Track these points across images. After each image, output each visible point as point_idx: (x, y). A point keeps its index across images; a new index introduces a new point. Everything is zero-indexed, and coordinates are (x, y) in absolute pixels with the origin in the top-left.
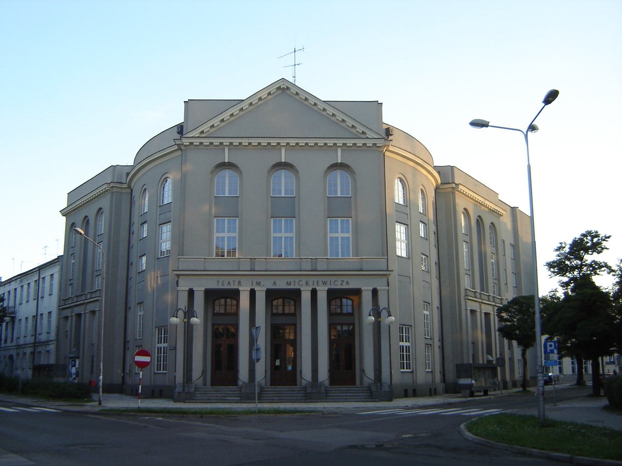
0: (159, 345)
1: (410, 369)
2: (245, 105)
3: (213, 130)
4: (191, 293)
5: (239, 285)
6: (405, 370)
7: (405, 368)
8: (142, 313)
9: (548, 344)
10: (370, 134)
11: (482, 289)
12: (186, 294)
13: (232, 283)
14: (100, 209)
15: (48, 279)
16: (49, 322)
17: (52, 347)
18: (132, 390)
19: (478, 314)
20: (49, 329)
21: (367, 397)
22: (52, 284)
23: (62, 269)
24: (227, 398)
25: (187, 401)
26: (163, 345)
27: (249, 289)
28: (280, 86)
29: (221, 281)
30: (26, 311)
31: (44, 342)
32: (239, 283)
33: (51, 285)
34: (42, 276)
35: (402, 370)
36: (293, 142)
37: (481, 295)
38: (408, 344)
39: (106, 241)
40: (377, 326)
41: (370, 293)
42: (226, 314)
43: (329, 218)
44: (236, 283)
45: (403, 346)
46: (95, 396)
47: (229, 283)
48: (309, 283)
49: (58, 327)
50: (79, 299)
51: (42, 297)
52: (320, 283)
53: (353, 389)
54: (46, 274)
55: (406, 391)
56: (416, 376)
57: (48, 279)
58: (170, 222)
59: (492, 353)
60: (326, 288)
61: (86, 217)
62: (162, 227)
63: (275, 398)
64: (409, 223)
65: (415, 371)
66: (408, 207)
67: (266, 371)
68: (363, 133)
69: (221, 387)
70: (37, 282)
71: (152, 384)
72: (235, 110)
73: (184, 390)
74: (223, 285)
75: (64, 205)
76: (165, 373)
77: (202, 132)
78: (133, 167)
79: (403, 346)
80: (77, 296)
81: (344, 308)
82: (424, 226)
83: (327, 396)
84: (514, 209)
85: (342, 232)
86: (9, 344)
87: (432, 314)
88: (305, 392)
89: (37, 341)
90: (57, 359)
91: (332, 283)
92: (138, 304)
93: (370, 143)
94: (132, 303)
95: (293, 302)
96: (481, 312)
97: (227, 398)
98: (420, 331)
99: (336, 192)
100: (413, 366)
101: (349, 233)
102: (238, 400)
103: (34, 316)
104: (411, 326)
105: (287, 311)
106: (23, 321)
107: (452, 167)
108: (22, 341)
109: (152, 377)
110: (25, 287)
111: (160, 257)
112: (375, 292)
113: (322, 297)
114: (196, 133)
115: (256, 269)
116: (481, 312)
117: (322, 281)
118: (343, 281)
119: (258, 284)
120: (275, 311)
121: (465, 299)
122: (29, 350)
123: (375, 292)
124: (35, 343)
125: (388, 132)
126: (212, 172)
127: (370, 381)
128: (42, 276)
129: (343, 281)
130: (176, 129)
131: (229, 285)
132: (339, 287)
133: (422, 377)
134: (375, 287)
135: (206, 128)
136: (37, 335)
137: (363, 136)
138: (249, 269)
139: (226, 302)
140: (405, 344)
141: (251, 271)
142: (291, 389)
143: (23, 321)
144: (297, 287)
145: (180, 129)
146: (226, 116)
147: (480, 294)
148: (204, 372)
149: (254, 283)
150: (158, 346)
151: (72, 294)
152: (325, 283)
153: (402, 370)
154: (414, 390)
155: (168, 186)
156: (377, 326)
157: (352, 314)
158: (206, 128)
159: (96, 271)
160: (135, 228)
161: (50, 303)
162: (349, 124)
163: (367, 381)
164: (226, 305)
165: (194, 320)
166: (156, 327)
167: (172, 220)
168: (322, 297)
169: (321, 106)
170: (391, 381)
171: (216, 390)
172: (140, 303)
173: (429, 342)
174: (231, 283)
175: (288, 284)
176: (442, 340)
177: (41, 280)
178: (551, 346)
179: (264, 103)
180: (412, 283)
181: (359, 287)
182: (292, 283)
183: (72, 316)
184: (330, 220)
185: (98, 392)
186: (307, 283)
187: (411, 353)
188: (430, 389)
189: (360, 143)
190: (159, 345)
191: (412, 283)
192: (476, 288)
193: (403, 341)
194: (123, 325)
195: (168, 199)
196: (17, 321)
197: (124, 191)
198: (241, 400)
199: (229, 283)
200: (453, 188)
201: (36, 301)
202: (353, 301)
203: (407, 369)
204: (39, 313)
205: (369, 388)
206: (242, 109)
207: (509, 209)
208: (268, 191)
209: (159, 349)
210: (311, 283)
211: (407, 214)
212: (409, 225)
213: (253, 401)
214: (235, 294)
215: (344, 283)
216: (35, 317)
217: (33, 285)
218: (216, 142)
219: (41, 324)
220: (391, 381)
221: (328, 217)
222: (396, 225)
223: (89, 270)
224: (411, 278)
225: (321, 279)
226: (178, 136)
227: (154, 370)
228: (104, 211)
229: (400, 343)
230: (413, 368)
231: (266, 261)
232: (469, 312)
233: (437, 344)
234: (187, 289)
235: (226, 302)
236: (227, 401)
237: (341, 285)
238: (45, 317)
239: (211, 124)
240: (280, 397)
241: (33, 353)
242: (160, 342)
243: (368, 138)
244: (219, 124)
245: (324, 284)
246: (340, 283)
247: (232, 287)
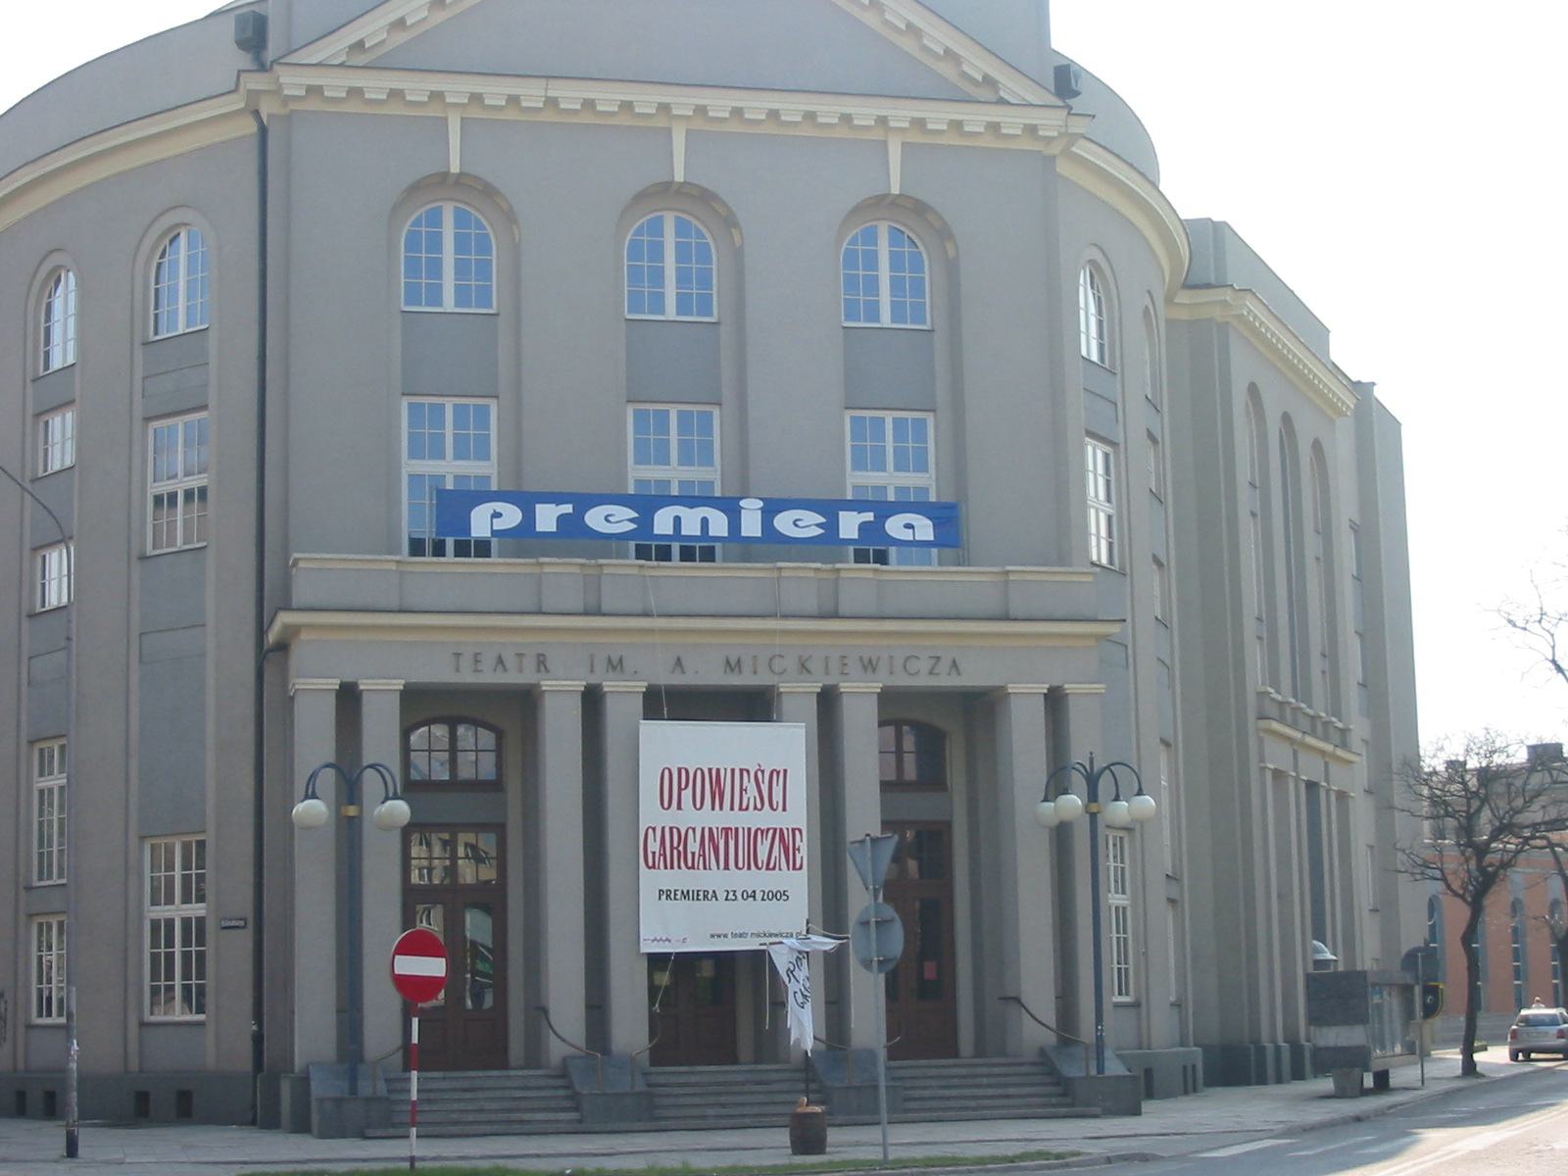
1: (1127, 994)
3: (401, 37)
4: (349, 698)
5: (539, 671)
8: (56, 781)
10: (1012, 86)
12: (330, 704)
13: (510, 661)
21: (1054, 1100)
24: (527, 1116)
25: (370, 1132)
26: (178, 911)
32: (541, 662)
38: (196, 910)
41: (1040, 704)
43: (405, 398)
44: (530, 663)
45: (170, 924)
48: (809, 665)
53: (985, 1070)
55: (21, 1096)
56: (1149, 1028)
59: (1324, 935)
62: (47, 423)
63: (710, 1112)
64: (1121, 439)
65: (1144, 1001)
66: (1119, 377)
68: (989, 82)
69: (481, 1074)
71: (21, 1066)
74: (476, 671)
76: (201, 1024)
77: (359, 46)
79: (170, 924)
81: (466, 760)
82: (1106, 456)
85: (460, 455)
88: (569, 1092)
95: (493, 735)
97: (527, 1116)
100: (1137, 983)
101: (487, 458)
102: (570, 1122)
105: (466, 772)
109: (133, 1047)
111: (150, 551)
112: (1055, 700)
114: (334, 48)
115: (605, 608)
117: (861, 658)
119: (616, 666)
120: (487, 842)
123: (1055, 700)
125: (1066, 81)
127: (570, 1051)
129: (938, 658)
131: (678, 669)
132: (924, 681)
134: (1056, 683)
135: (372, 28)
137: (984, 94)
138: (811, 605)
139: (453, 737)
141: (586, 614)
142: (721, 1078)
149: (600, 665)
150: (154, 916)
152: (869, 666)
157: (496, 786)
162: (932, 46)
163: (556, 1050)
164: (453, 749)
167: (212, 402)
171: (466, 1084)
174: (508, 665)
180: (1131, 668)
182: (747, 668)
184: (636, 412)
186: (803, 667)
187: (1130, 935)
188: (1185, 1068)
190: (162, 912)
191: (1131, 668)
193: (186, 922)
198: (580, 1121)
199: (500, 661)
202: (500, 735)
205: (563, 1072)
209: (162, 931)
212: (1122, 445)
213: (867, 1118)
215: (944, 666)
221: (403, 394)
222: (1090, 449)
224: (1130, 651)
226: (244, 60)
229: (202, 913)
231: (402, 573)
235: (453, 737)
236: (527, 1128)
240: (723, 1105)
242: (162, 894)
243: (1002, 102)
244: (424, 19)
245: (865, 668)
246: (924, 665)
247: (511, 678)
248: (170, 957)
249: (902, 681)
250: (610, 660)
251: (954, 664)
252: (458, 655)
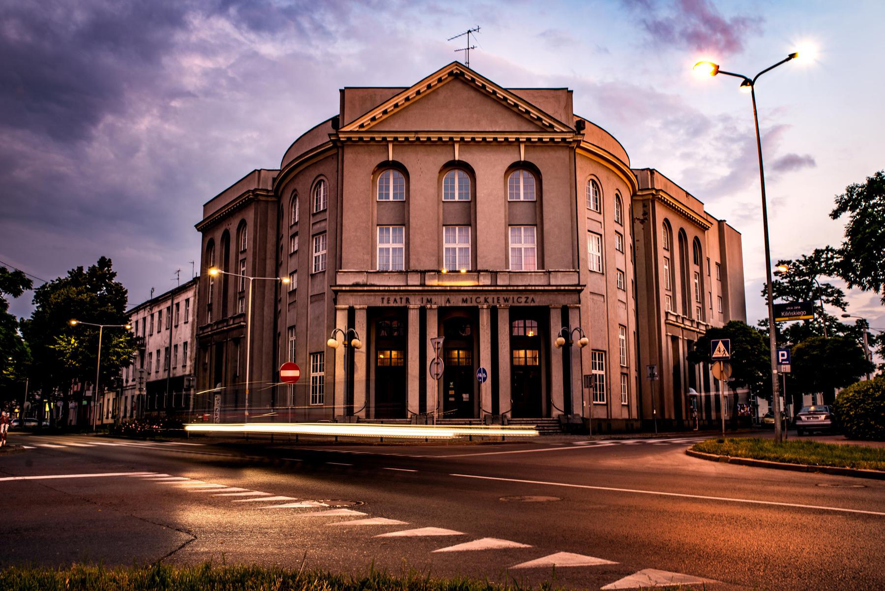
0: (315, 374)
2: (411, 93)
6: (598, 402)
9: (780, 353)
11: (684, 313)
13: (399, 300)
26: (318, 374)
28: (452, 71)
29: (386, 298)
32: (407, 300)
36: (468, 137)
39: (250, 259)
40: (567, 348)
44: (404, 301)
47: (395, 300)
50: (220, 326)
51: (176, 326)
52: (502, 301)
54: (181, 299)
67: (439, 402)
72: (400, 99)
77: (362, 126)
78: (281, 171)
84: (721, 223)
86: (130, 383)
92: (289, 328)
93: (558, 137)
94: (281, 328)
98: (615, 361)
99: (518, 195)
104: (605, 352)
107: (652, 171)
125: (581, 124)
126: (374, 173)
127: (560, 413)
128: (175, 302)
133: (619, 412)
137: (549, 130)
138: (418, 283)
140: (318, 374)
145: (335, 122)
146: (389, 106)
147: (683, 318)
149: (425, 301)
151: (211, 320)
156: (567, 348)
160: (284, 241)
165: (354, 342)
166: (310, 354)
172: (292, 328)
173: (625, 371)
175: (464, 301)
176: (639, 370)
178: (783, 355)
179: (434, 91)
189: (546, 137)
190: (315, 374)
192: (29, 272)
196: (147, 355)
197: (269, 199)
199: (395, 300)
200: (652, 194)
201: (169, 331)
206: (407, 99)
207: (715, 223)
208: (439, 195)
217: (165, 311)
218: (378, 137)
223: (231, 292)
225: (502, 297)
233: (633, 373)
237: (526, 302)
243: (556, 132)
246: (523, 300)
251: (533, 300)
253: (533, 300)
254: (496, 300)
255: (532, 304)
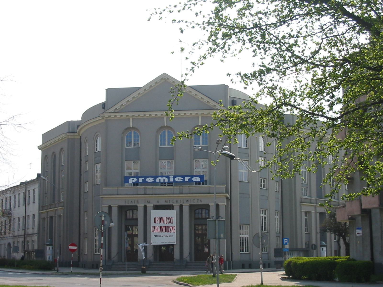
1: (248, 251)
2: (141, 91)
7: (244, 251)
13: (133, 202)
14: (62, 149)
15: (32, 192)
16: (34, 221)
17: (36, 238)
18: (82, 265)
19: (313, 215)
20: (33, 228)
22: (35, 194)
23: (40, 186)
27: (143, 205)
30: (18, 212)
31: (31, 234)
32: (138, 202)
33: (34, 196)
34: (28, 189)
35: (262, 252)
37: (316, 202)
42: (133, 219)
44: (136, 202)
46: (56, 269)
49: (39, 224)
54: (31, 188)
57: (32, 192)
58: (100, 163)
60: (188, 204)
61: (54, 152)
70: (25, 193)
72: (135, 95)
73: (105, 264)
75: (40, 143)
80: (50, 205)
83: (186, 267)
87: (269, 216)
89: (26, 233)
90: (39, 246)
91: (192, 201)
96: (316, 212)
103: (23, 217)
106: (17, 220)
108: (16, 234)
110: (17, 196)
113: (186, 210)
114: (112, 110)
116: (316, 212)
118: (198, 200)
119: (149, 202)
120: (197, 217)
121: (301, 205)
122: (21, 240)
124: (25, 235)
130: (101, 106)
136: (26, 229)
138: (143, 193)
141: (144, 194)
143: (17, 220)
144: (171, 203)
145: (104, 105)
148: (190, 253)
152: (187, 201)
153: (262, 252)
154: (269, 264)
155: (99, 140)
158: (118, 106)
159: (61, 189)
161: (34, 209)
168: (186, 210)
169: (188, 90)
170: (79, 257)
177: (27, 192)
180: (250, 198)
181: (207, 203)
183: (47, 218)
185: (56, 266)
186: (177, 201)
194: (78, 225)
195: (99, 149)
203: (245, 251)
204: (27, 215)
210: (179, 201)
211: (248, 154)
214: (135, 208)
216: (24, 218)
217: (22, 195)
219: (29, 222)
220: (79, 257)
227: (94, 253)
228: (64, 148)
230: (250, 251)
232: (303, 214)
234: (108, 206)
237: (197, 202)
238: (31, 217)
239: (122, 104)
241: (24, 242)
246: (196, 201)
248: (245, 246)
249: (192, 203)
250: (165, 201)
251: (201, 200)
252: (125, 201)
253: (201, 200)
254: (182, 201)
255: (199, 203)
